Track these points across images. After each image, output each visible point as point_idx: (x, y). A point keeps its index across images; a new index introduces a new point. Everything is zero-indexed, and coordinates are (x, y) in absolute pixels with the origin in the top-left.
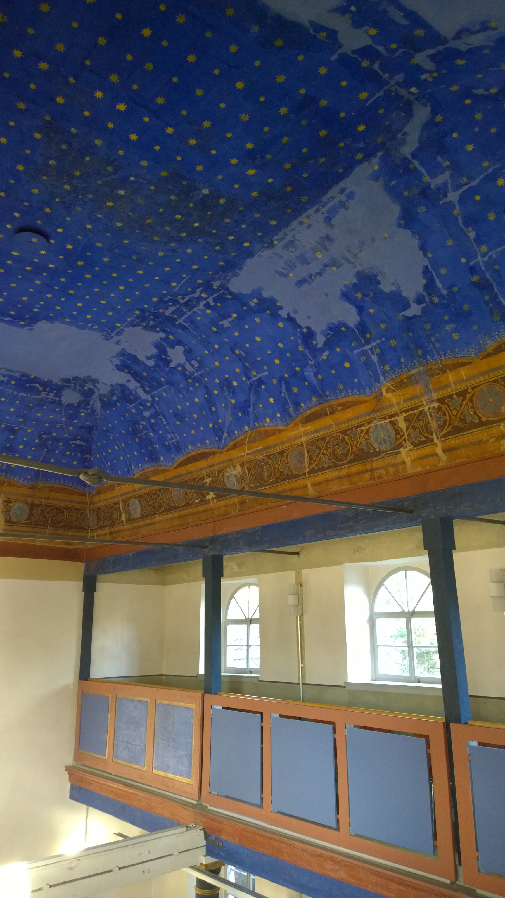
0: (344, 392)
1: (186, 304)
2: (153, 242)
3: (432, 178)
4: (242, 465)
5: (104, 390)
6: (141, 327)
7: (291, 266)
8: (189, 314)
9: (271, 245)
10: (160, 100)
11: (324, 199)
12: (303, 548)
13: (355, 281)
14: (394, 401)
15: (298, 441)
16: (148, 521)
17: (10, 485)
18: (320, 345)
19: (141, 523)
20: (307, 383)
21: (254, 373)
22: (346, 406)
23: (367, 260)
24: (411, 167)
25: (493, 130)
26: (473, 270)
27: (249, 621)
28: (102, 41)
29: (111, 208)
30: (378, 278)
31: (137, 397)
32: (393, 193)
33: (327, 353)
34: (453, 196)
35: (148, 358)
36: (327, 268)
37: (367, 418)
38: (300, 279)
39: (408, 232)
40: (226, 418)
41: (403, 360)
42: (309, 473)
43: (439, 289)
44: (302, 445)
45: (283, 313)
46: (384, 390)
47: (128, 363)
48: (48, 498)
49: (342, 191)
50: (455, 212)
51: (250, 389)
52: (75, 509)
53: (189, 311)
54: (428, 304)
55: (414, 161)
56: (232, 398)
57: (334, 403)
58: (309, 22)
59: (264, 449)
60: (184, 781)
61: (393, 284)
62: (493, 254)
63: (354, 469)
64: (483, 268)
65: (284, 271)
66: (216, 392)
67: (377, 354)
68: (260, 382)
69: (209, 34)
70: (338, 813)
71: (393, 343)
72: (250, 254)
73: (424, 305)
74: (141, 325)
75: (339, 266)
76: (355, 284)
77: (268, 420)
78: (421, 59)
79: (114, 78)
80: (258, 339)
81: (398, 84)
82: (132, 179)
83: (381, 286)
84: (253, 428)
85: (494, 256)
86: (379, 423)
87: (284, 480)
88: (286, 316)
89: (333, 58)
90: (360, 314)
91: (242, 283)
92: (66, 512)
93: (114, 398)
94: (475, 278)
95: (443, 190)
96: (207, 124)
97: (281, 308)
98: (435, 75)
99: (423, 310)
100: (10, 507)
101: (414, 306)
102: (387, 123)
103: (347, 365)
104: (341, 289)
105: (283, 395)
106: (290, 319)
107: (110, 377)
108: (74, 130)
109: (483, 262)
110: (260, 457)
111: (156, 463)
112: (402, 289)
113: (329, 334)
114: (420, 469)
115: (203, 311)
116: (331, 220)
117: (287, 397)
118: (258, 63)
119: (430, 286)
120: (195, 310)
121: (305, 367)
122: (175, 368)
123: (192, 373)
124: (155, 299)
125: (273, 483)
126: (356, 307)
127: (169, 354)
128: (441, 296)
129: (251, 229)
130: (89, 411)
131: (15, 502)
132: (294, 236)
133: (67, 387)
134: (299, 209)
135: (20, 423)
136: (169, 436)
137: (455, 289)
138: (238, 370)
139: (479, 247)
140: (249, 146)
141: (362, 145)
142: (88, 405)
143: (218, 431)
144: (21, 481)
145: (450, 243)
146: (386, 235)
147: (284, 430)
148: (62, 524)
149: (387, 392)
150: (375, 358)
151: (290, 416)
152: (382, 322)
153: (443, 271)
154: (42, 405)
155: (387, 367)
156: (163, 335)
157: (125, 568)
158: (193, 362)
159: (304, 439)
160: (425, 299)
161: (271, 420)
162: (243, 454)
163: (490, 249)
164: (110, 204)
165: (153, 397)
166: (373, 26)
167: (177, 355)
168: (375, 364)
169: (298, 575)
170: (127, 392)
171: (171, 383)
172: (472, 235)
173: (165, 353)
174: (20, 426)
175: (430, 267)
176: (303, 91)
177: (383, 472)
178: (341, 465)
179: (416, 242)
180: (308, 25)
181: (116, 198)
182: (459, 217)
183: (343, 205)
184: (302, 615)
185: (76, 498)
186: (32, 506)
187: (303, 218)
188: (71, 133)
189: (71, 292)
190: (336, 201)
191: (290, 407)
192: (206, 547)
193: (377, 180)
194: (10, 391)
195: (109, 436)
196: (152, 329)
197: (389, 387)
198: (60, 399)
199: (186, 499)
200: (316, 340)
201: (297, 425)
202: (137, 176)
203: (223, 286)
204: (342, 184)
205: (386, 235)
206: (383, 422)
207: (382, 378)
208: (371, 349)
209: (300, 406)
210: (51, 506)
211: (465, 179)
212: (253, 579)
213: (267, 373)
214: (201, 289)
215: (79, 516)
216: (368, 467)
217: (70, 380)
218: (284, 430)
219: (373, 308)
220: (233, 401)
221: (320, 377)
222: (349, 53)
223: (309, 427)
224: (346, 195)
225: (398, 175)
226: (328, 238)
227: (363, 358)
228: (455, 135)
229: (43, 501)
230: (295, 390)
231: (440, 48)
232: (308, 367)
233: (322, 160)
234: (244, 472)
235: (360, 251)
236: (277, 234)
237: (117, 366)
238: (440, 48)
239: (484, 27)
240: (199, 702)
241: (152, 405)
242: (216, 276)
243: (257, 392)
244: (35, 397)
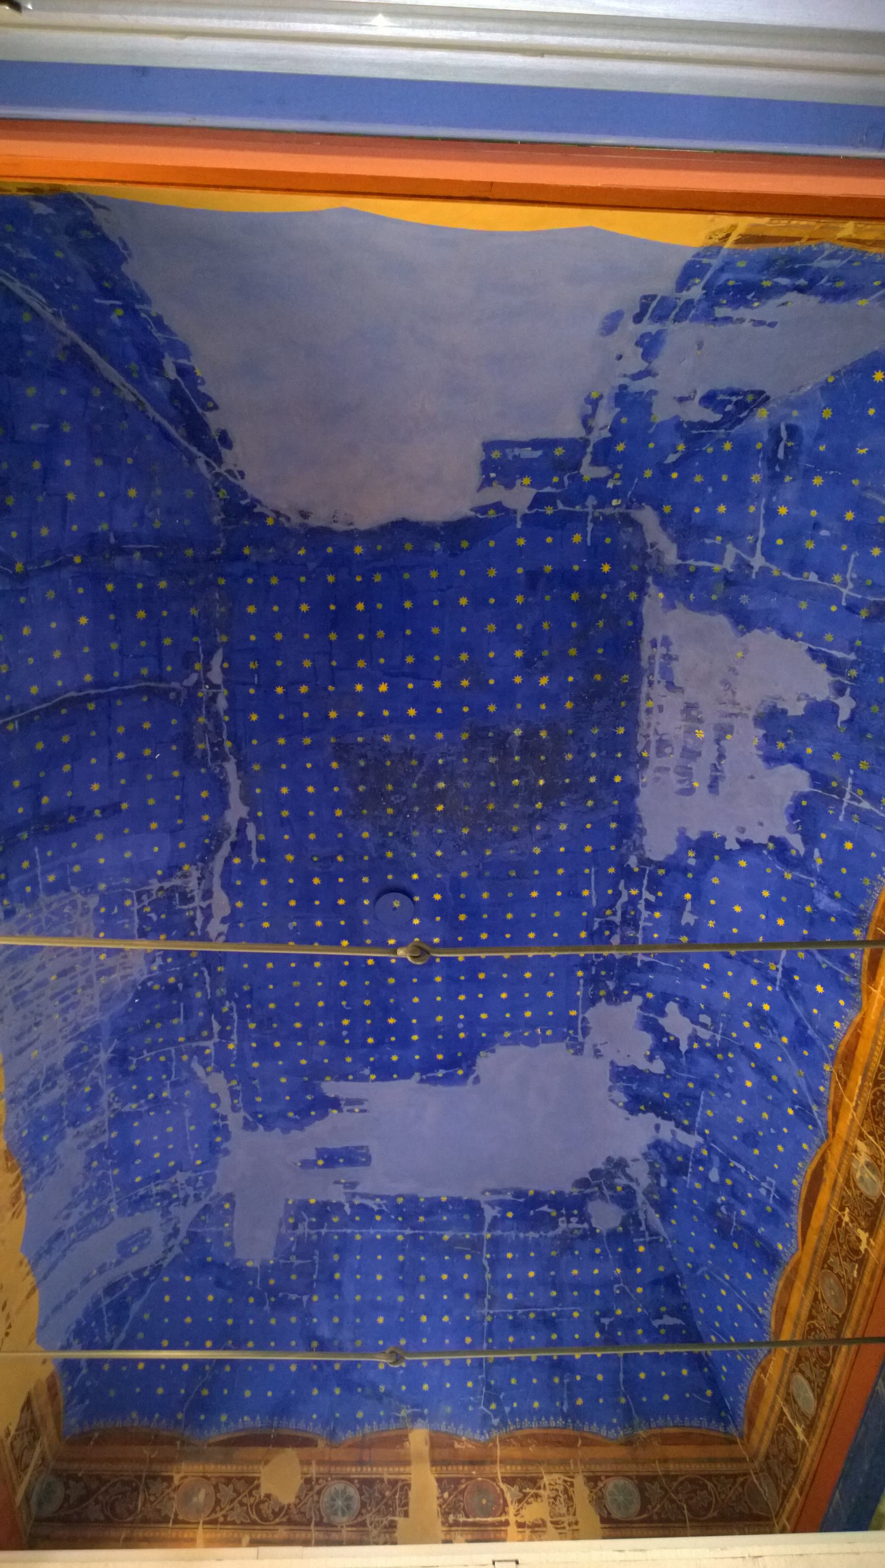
0: (875, 884)
1: (625, 921)
2: (515, 836)
3: (721, 563)
4: (861, 1137)
6: (603, 1000)
7: (686, 773)
9: (644, 763)
10: (410, 659)
11: (644, 663)
13: (762, 732)
17: (588, 1443)
18: (802, 851)
20: (833, 919)
23: (751, 697)
24: (692, 569)
25: (725, 478)
26: (852, 608)
28: (333, 636)
29: (444, 811)
30: (779, 706)
32: (704, 606)
33: (816, 852)
34: (758, 561)
35: (651, 1059)
36: (722, 743)
38: (709, 782)
39: (757, 632)
40: (795, 1074)
43: (845, 660)
45: (731, 845)
47: (639, 1093)
48: (665, 1461)
49: (654, 644)
50: (776, 573)
51: (787, 997)
52: (727, 1476)
54: (852, 687)
55: (688, 562)
56: (780, 1036)
58: (472, 510)
61: (799, 699)
62: (851, 574)
64: (859, 596)
65: (685, 785)
67: (863, 797)
68: (788, 973)
69: (406, 576)
71: (864, 765)
72: (631, 791)
73: (848, 690)
74: (601, 997)
75: (730, 730)
76: (765, 736)
77: (837, 1024)
78: (589, 472)
79: (361, 664)
81: (595, 507)
82: (440, 761)
83: (791, 713)
84: (833, 1058)
85: (855, 576)
88: (736, 847)
89: (519, 525)
90: (803, 767)
91: (659, 842)
92: (710, 1485)
94: (864, 613)
95: (742, 565)
96: (464, 657)
97: (723, 839)
98: (617, 476)
99: (853, 696)
100: (601, 1490)
101: (840, 701)
102: (625, 547)
103: (849, 846)
104: (759, 756)
105: (824, 966)
106: (746, 846)
108: (360, 739)
109: (851, 590)
111: (779, 1264)
112: (812, 696)
113: (798, 825)
115: (650, 919)
116: (673, 683)
117: (830, 964)
118: (462, 573)
119: (834, 666)
121: (813, 898)
122: (690, 1051)
123: (712, 1040)
126: (791, 761)
127: (668, 1030)
128: (854, 664)
129: (604, 753)
130: (648, 1239)
131: (607, 1477)
132: (656, 732)
133: (590, 1196)
134: (632, 696)
135: (555, 1301)
137: (858, 643)
139: (832, 582)
140: (519, 654)
141: (623, 584)
142: (640, 1224)
143: (804, 1114)
144: (604, 1432)
145: (803, 605)
146: (740, 654)
147: (863, 1019)
148: (712, 1514)
150: (866, 805)
151: (853, 989)
152: (831, 753)
153: (829, 637)
154: (571, 1249)
156: (637, 1000)
160: (843, 684)
161: (841, 1021)
162: (850, 1117)
163: (844, 573)
164: (440, 808)
165: (703, 1135)
166: (522, 476)
167: (675, 1022)
168: (871, 812)
170: (669, 1152)
171: (704, 1084)
172: (813, 577)
174: (558, 1309)
175: (814, 648)
176: (520, 570)
179: (773, 635)
180: (473, 514)
181: (440, 796)
182: (784, 574)
183: (668, 658)
185: (720, 1451)
186: (642, 1481)
187: (645, 704)
188: (358, 744)
190: (658, 661)
191: (844, 976)
193: (674, 607)
194: (513, 1234)
195: (702, 1277)
198: (590, 1224)
199: (844, 1286)
200: (793, 848)
201: (869, 993)
202: (443, 756)
203: (644, 861)
204: (646, 636)
205: (740, 654)
208: (853, 798)
209: (852, 961)
210: (677, 1477)
211: (750, 538)
214: (622, 883)
215: (740, 1489)
217: (586, 1180)
218: (863, 1019)
219: (808, 746)
221: (837, 894)
222: (527, 511)
224: (662, 645)
225: (685, 586)
226: (689, 707)
227: (855, 819)
228: (697, 510)
229: (659, 1469)
231: (590, 449)
232: (816, 894)
233: (601, 624)
235: (734, 693)
236: (637, 743)
237: (626, 1106)
238: (590, 449)
239: (594, 403)
242: (623, 850)
243: (797, 995)
244: (551, 1234)
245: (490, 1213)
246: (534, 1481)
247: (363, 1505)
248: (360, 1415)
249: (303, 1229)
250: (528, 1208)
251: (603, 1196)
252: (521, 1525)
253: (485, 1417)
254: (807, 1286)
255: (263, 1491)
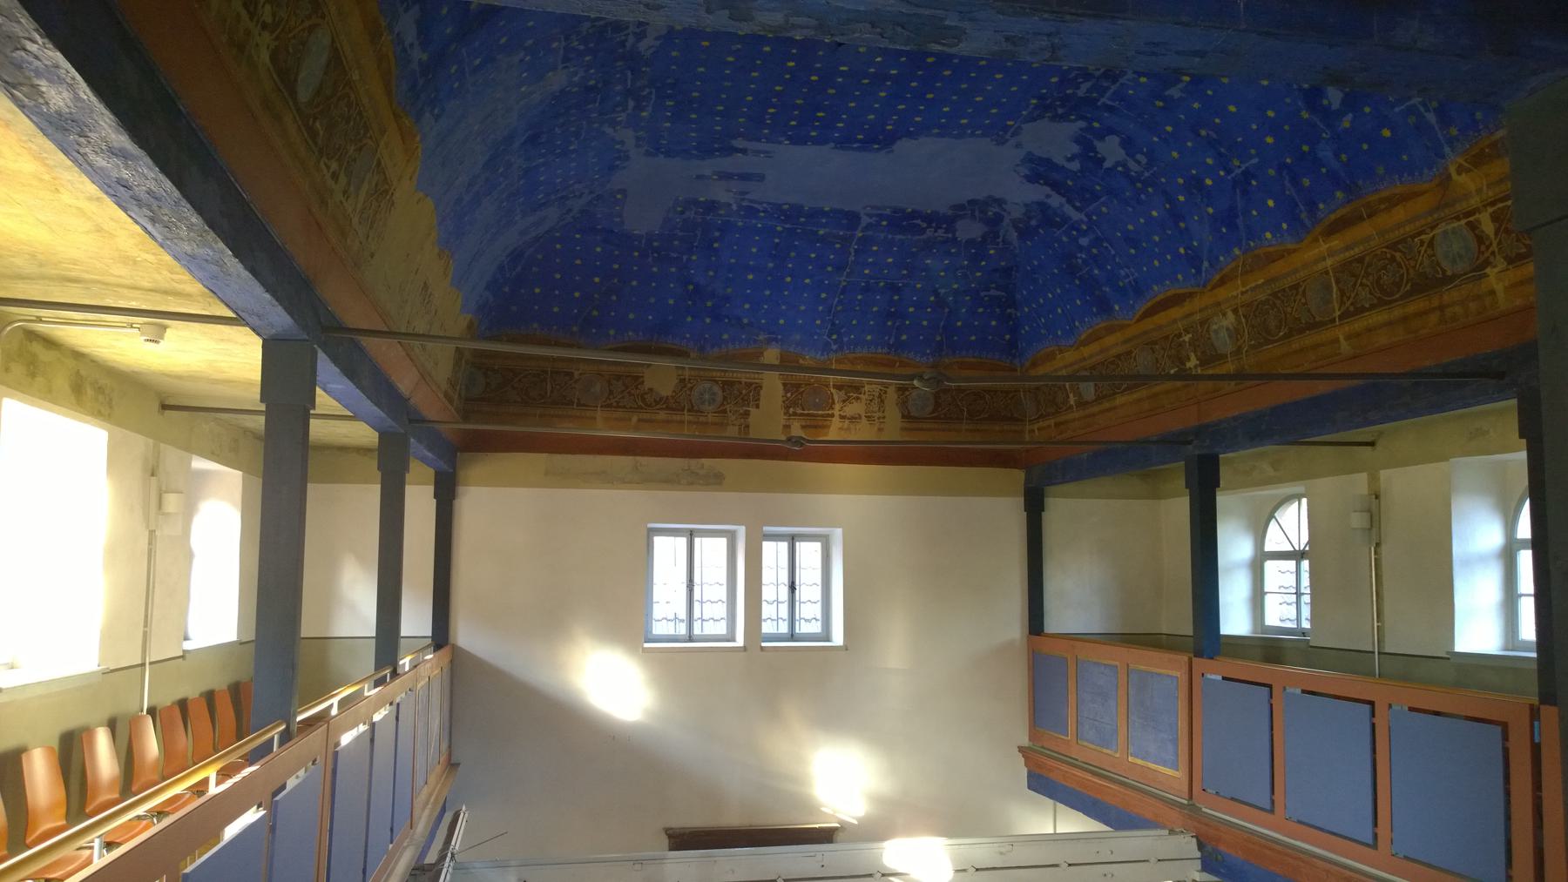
4: (1235, 311)
5: (1017, 213)
8: (1114, 88)
12: (1381, 433)
14: (1472, 187)
15: (1320, 266)
16: (1107, 405)
18: (1336, 105)
19: (1095, 409)
21: (1237, 163)
22: (1392, 202)
27: (1297, 556)
31: (1066, 219)
35: (1069, 160)
37: (1430, 219)
41: (1479, 115)
42: (1341, 318)
44: (1327, 273)
46: (1452, 170)
47: (1040, 170)
53: (1114, 82)
57: (1373, 198)
59: (1268, 282)
60: (1171, 774)
63: (1411, 308)
66: (1182, 198)
68: (1248, 175)
70: (1376, 825)
77: (1268, 235)
80: (1232, 109)
86: (1449, 227)
87: (1301, 331)
93: (1033, 223)
103: (1386, 133)
107: (1020, 194)
110: (1262, 297)
114: (1518, 302)
120: (1121, 81)
124: (1054, 80)
125: (1286, 336)
136: (1123, 273)
138: (1209, 161)
143: (1194, 260)
149: (1459, 174)
150: (1431, 118)
155: (1454, 131)
156: (1082, 124)
157: (1078, 477)
158: (1139, 157)
159: (1329, 262)
161: (1274, 235)
167: (1111, 150)
169: (1374, 479)
173: (1094, 149)
177: (1458, 309)
178: (1391, 302)
184: (1378, 545)
189: (930, 96)
192: (1189, 443)
194: (882, 235)
196: (1062, 118)
197: (1460, 166)
201: (1316, 240)
206: (1456, 224)
207: (1447, 150)
212: (1298, 488)
213: (1255, 161)
216: (1436, 303)
220: (1210, 210)
221: (1344, 157)
223: (1336, 242)
227: (1412, 120)
230: (1306, 182)
234: (1240, 322)
237: (1026, 177)
240: (1185, 669)
241: (1089, 228)
245: (865, 220)
246: (857, 388)
247: (725, 398)
248: (725, 336)
249: (690, 214)
250: (902, 220)
251: (973, 216)
252: (842, 417)
253: (827, 344)
254: (1125, 342)
255: (647, 385)
